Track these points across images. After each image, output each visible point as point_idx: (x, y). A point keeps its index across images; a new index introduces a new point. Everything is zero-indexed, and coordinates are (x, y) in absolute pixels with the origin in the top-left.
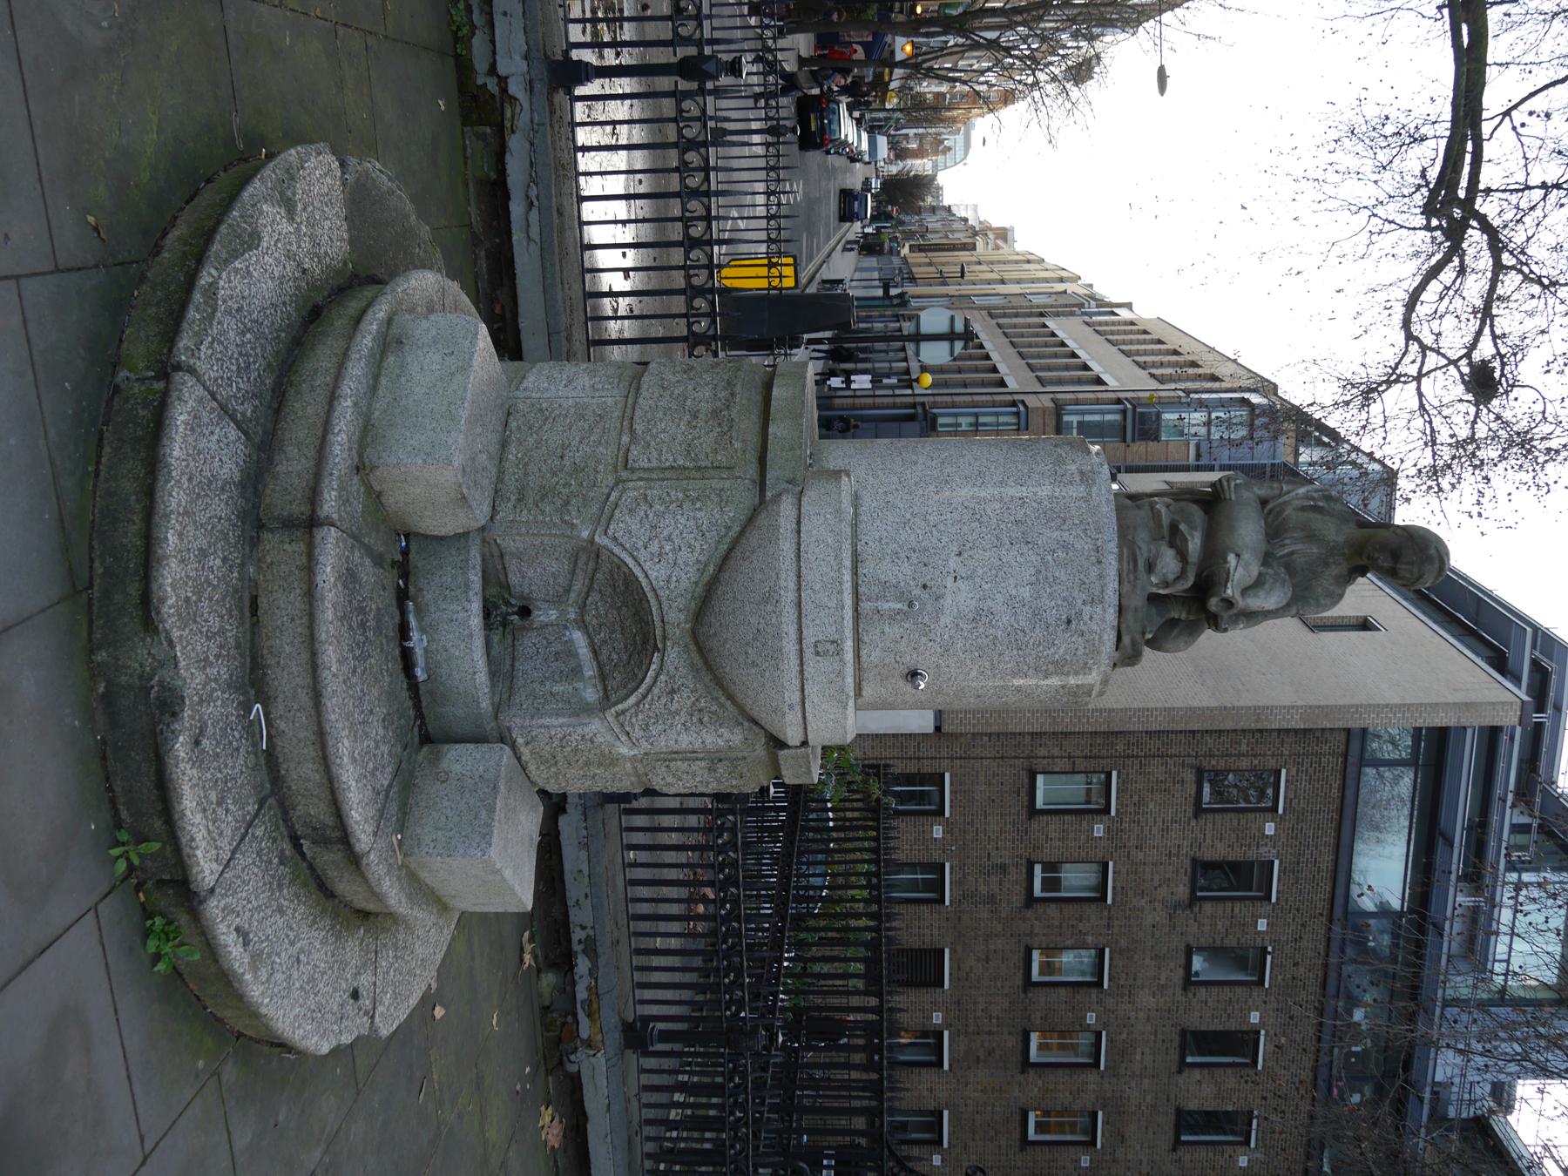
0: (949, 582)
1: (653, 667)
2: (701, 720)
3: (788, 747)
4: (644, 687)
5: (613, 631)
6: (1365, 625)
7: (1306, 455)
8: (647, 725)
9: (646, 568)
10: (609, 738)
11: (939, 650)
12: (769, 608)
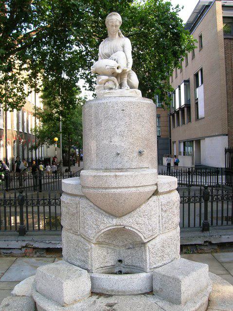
0: (112, 144)
1: (129, 228)
6: (201, 37)
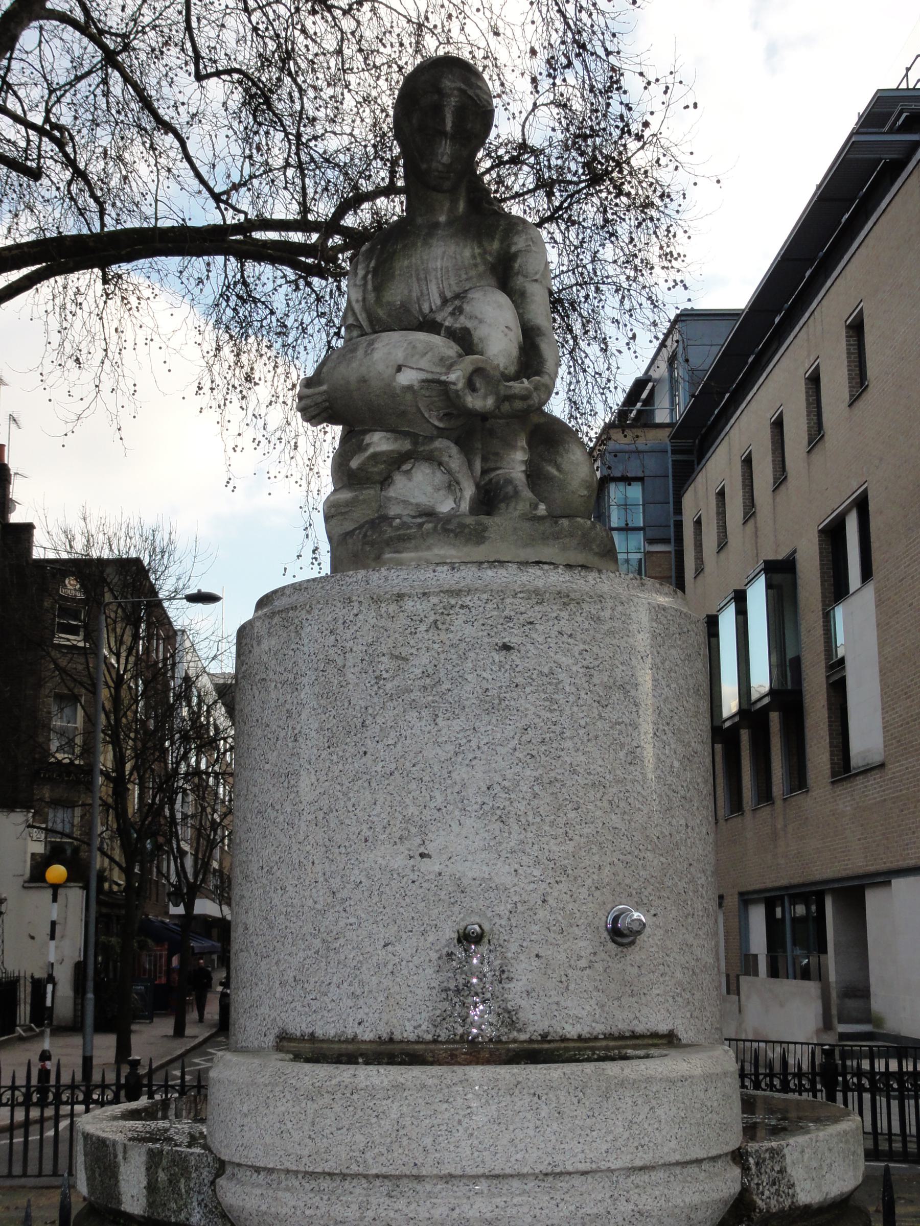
0: (431, 867)
3: (745, 1191)
6: (856, 329)
7: (662, 416)
11: (563, 887)
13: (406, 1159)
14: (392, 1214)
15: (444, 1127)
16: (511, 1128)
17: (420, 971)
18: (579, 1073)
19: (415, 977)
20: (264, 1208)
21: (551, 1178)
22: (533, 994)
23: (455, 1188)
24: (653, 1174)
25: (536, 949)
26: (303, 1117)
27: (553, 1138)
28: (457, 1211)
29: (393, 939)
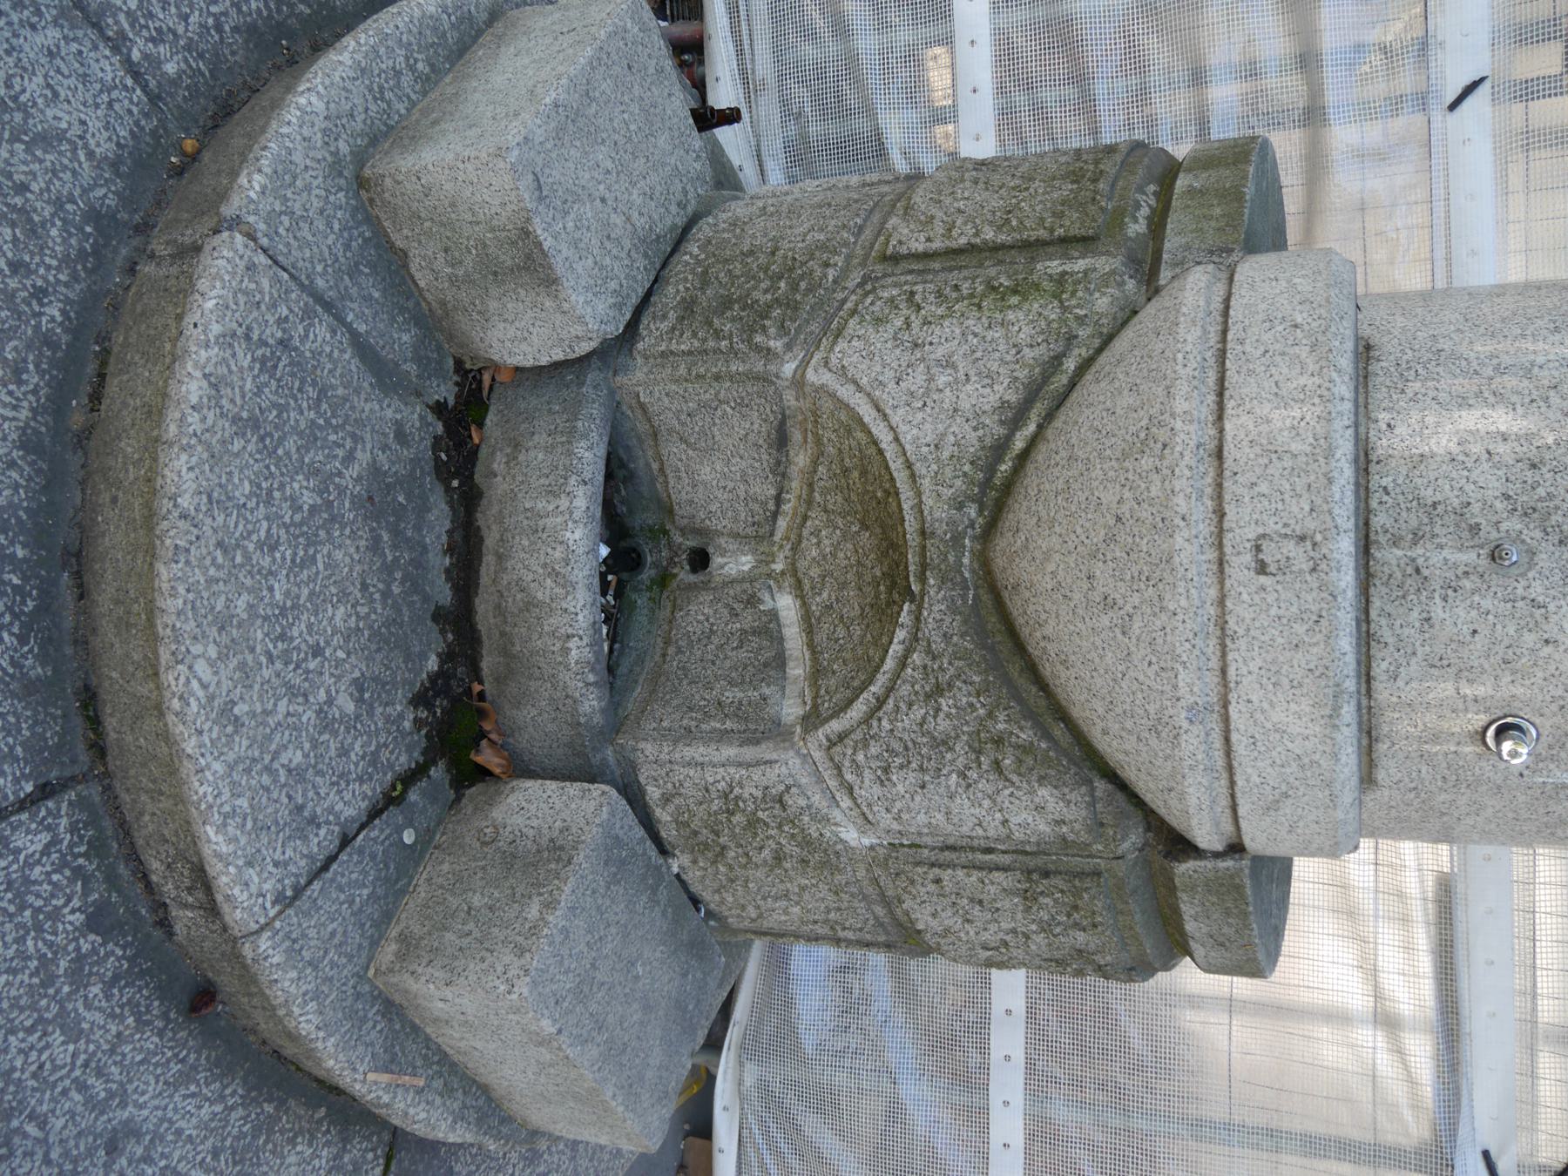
1: (900, 634)
2: (997, 766)
4: (881, 680)
5: (843, 585)
8: (886, 770)
9: (895, 419)
10: (817, 799)
12: (1146, 463)
13: (1241, 463)
14: (1178, 449)
15: (1280, 506)
16: (1279, 587)
17: (1455, 492)
18: (1345, 672)
19: (1448, 486)
20: (1184, 310)
21: (1218, 633)
22: (1426, 626)
23: (1208, 521)
24: (1221, 753)
25: (1484, 631)
26: (1289, 342)
27: (1266, 638)
28: (1182, 524)
29: (1497, 458)
